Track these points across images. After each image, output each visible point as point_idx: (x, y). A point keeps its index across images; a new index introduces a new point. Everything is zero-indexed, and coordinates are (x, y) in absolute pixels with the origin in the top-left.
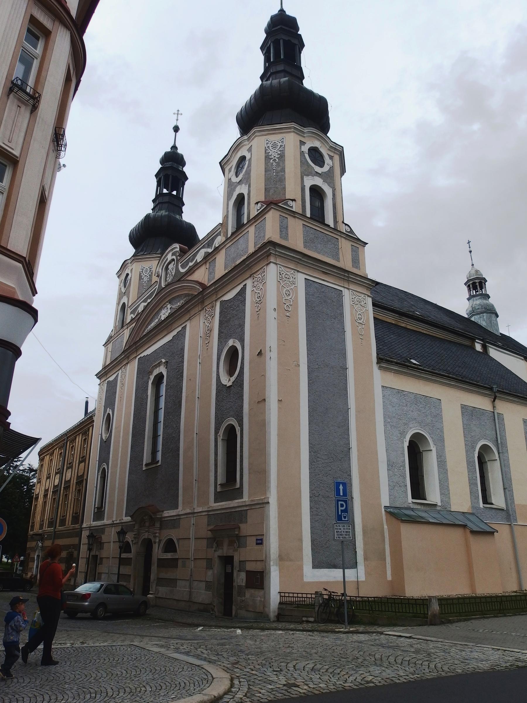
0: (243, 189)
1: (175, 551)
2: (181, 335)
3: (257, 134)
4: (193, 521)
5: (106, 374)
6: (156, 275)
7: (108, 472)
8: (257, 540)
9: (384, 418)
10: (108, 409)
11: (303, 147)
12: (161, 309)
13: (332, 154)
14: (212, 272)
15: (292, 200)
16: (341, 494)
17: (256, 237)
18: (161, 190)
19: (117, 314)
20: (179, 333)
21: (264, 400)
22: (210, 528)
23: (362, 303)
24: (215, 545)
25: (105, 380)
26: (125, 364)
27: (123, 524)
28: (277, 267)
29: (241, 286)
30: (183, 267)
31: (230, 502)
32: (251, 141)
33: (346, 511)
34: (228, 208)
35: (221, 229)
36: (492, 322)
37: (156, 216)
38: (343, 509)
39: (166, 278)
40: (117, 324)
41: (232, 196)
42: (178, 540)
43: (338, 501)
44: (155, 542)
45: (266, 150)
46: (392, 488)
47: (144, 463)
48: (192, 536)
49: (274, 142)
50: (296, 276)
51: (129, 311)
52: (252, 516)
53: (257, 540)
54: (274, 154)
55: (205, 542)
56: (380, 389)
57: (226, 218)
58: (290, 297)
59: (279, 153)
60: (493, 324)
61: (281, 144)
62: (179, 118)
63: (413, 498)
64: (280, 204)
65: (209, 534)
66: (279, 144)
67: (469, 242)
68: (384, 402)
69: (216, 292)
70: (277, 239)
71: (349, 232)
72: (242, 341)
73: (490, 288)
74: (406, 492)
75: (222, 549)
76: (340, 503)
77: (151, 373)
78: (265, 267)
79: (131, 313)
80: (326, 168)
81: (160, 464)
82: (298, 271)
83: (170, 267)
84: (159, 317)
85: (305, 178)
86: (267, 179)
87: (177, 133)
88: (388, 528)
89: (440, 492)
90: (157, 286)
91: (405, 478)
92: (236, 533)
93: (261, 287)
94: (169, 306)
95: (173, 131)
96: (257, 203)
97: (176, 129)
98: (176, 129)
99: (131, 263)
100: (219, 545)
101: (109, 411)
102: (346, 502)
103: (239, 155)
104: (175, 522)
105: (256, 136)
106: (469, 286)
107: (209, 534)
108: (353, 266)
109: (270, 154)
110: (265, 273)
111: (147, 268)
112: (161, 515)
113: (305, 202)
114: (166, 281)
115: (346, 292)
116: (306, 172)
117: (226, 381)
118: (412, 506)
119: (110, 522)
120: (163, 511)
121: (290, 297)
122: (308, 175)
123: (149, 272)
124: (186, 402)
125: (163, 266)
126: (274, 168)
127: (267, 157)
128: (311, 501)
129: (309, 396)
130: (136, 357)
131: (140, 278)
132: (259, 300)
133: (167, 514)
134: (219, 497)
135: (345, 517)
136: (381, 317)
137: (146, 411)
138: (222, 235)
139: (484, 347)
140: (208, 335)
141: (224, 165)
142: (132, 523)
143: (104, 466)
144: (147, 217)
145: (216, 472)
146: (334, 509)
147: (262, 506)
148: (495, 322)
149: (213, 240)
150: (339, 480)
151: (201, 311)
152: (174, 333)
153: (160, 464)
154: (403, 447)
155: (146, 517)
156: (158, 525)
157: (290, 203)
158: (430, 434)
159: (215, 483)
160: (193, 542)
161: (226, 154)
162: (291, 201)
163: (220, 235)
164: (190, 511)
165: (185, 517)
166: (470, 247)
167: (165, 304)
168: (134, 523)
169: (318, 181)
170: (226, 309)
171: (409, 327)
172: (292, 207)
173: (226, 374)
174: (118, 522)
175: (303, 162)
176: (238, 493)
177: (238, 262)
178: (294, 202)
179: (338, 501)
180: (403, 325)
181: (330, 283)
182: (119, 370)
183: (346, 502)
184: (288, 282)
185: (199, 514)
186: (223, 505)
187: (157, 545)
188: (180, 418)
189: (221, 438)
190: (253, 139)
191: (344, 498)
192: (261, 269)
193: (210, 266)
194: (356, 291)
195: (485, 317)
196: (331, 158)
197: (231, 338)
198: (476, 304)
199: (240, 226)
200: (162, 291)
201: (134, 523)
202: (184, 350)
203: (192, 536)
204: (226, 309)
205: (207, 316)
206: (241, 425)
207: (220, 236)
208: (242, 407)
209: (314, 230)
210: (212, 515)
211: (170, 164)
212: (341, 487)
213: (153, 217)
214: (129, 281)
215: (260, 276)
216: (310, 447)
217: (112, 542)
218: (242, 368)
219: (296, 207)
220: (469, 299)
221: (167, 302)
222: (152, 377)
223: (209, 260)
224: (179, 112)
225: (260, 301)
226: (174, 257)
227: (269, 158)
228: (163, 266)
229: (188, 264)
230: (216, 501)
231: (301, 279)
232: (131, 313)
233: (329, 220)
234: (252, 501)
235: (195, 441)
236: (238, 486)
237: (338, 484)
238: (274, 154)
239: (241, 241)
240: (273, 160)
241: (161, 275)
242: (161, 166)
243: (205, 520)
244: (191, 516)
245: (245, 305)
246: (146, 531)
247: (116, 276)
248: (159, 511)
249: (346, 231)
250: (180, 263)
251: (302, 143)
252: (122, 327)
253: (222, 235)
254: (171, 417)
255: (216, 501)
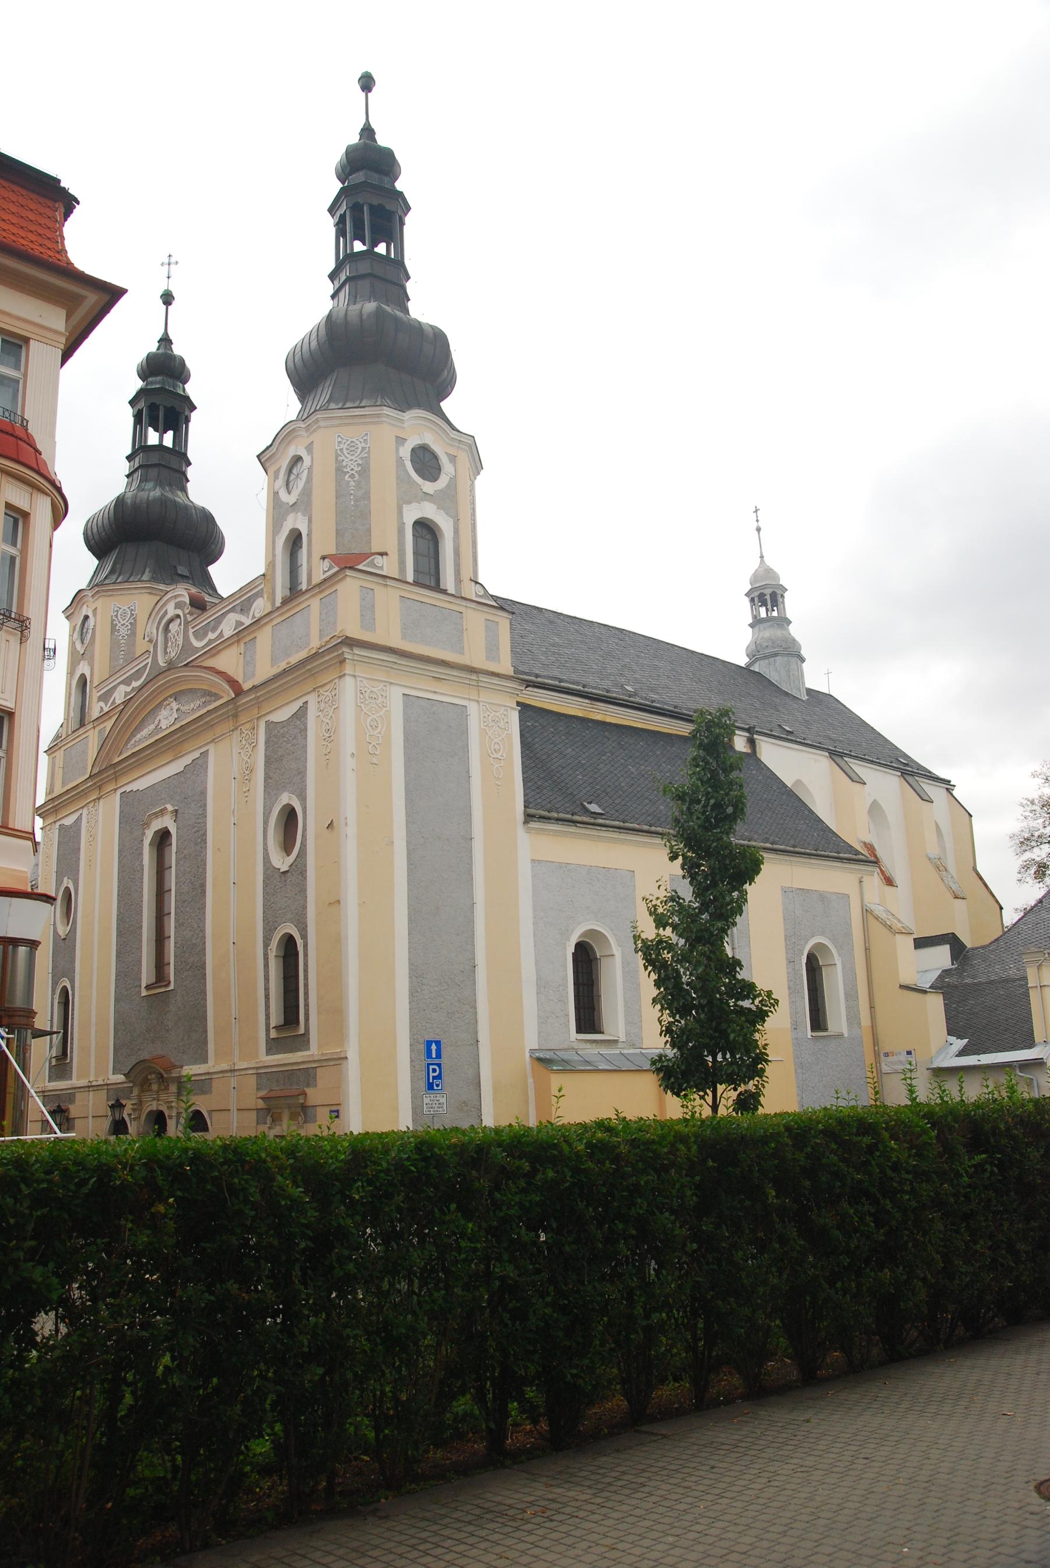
0: (297, 521)
1: (205, 1129)
2: (199, 766)
3: (322, 424)
4: (233, 1082)
5: (56, 810)
6: (147, 639)
7: (73, 995)
8: (331, 1111)
9: (534, 910)
10: (66, 879)
11: (401, 449)
12: (159, 706)
13: (452, 451)
14: (249, 663)
15: (382, 554)
16: (434, 1056)
17: (321, 620)
18: (144, 436)
19: (70, 694)
20: (196, 762)
21: (339, 901)
22: (262, 1093)
23: (501, 724)
24: (269, 1119)
25: (55, 822)
26: (95, 800)
27: (109, 1087)
28: (356, 681)
29: (299, 703)
30: (198, 635)
31: (290, 1055)
32: (312, 433)
33: (439, 1077)
34: (274, 548)
35: (262, 586)
36: (791, 673)
37: (138, 499)
38: (436, 1074)
39: (166, 648)
40: (72, 714)
41: (281, 527)
42: (210, 1112)
43: (429, 1065)
44: (171, 1117)
45: (337, 456)
46: (542, 1021)
47: (144, 985)
48: (233, 1107)
49: (351, 440)
50: (388, 693)
51: (96, 695)
52: (323, 1076)
53: (331, 1111)
54: (351, 463)
55: (253, 1115)
56: (529, 864)
57: (271, 565)
58: (378, 731)
59: (360, 462)
60: (792, 677)
61: (363, 445)
62: (171, 274)
63: (579, 1030)
64: (360, 567)
65: (261, 1104)
66: (360, 446)
67: (756, 511)
68: (534, 886)
69: (258, 703)
70: (355, 632)
71: (481, 596)
72: (303, 799)
73: (792, 605)
74: (567, 1025)
75: (281, 1125)
76: (431, 1067)
77: (146, 825)
78: (337, 681)
79: (100, 699)
80: (443, 482)
81: (172, 987)
82: (391, 683)
83: (174, 627)
84: (156, 722)
85: (405, 508)
86: (341, 513)
87: (169, 307)
88: (534, 1083)
89: (626, 1020)
90: (150, 660)
91: (566, 1003)
92: (301, 1101)
93: (331, 714)
94: (175, 705)
95: (161, 301)
96: (323, 558)
97: (168, 299)
98: (168, 299)
99: (92, 596)
100: (276, 1119)
101: (67, 883)
102: (439, 1065)
103: (292, 451)
104: (203, 1085)
105: (319, 427)
106: (752, 600)
107: (261, 1104)
108: (488, 658)
109: (344, 464)
110: (337, 691)
111: (126, 608)
112: (180, 1072)
113: (404, 554)
114: (166, 653)
115: (473, 709)
116: (407, 495)
117: (281, 862)
118: (576, 1045)
119: (84, 1082)
120: (182, 1067)
121: (378, 731)
122: (409, 502)
123: (129, 616)
124: (214, 885)
125: (159, 623)
126: (352, 492)
127: (340, 470)
128: (412, 1051)
129: (409, 890)
130: (115, 790)
131: (114, 628)
132: (328, 735)
133: (190, 1070)
134: (274, 1046)
135: (438, 1085)
136: (556, 706)
137: (141, 892)
138: (265, 596)
139: (752, 742)
140: (247, 777)
141: (266, 461)
142: (126, 1085)
143: (64, 984)
144: (120, 501)
145: (267, 1007)
146: (424, 1073)
147: (338, 1062)
148: (796, 673)
149: (250, 601)
150: (428, 1037)
151: (233, 730)
152: (188, 760)
153: (172, 987)
154: (565, 956)
155: (153, 1076)
156: (173, 1088)
157: (378, 560)
158: (612, 930)
159: (266, 1024)
160: (235, 1116)
161: (269, 444)
162: (379, 557)
163: (262, 596)
164: (228, 1068)
165: (220, 1075)
166: (757, 521)
167: (166, 699)
168: (131, 1085)
169: (429, 511)
170: (275, 736)
171: (609, 720)
172: (381, 568)
173: (279, 849)
174: (100, 1082)
175: (402, 479)
176: (303, 1042)
177: (294, 659)
178: (384, 557)
179: (429, 1065)
180: (599, 717)
181: (447, 693)
182: (82, 807)
183: (439, 1065)
184: (374, 706)
185: (243, 1073)
186: (280, 1060)
187: (174, 1120)
188: (204, 913)
189: (274, 954)
190: (314, 431)
191: (437, 1061)
192: (330, 682)
193: (246, 650)
194: (491, 703)
195: (777, 664)
196: (453, 459)
197: (284, 791)
198: (763, 638)
199: (294, 592)
200: (161, 677)
201: (131, 1085)
202: (206, 795)
203: (233, 1107)
204: (275, 736)
205: (244, 742)
206: (304, 937)
207: (261, 599)
208: (305, 907)
209: (419, 604)
210: (263, 1076)
211: (159, 383)
212: (434, 1047)
213: (132, 498)
214: (90, 631)
215: (328, 693)
216: (411, 970)
217: (91, 1118)
218: (304, 845)
219: (387, 566)
220: (752, 626)
221: (170, 696)
222: (149, 834)
223: (244, 637)
224: (173, 260)
225: (330, 736)
226: (179, 612)
227: (343, 472)
228: (159, 623)
229: (205, 635)
230: (269, 1052)
231: (395, 696)
232: (100, 699)
233: (448, 581)
234: (323, 1054)
235: (232, 957)
236: (302, 1031)
237: (429, 1043)
238: (351, 463)
239: (298, 619)
240: (350, 477)
241: (157, 640)
242: (139, 384)
243: (252, 1081)
244: (229, 1074)
245: (306, 738)
246: (154, 1099)
247: (63, 616)
248: (175, 1067)
249: (477, 595)
250: (193, 628)
251: (401, 441)
252: (82, 724)
253: (265, 596)
254: (188, 909)
255: (269, 1052)
